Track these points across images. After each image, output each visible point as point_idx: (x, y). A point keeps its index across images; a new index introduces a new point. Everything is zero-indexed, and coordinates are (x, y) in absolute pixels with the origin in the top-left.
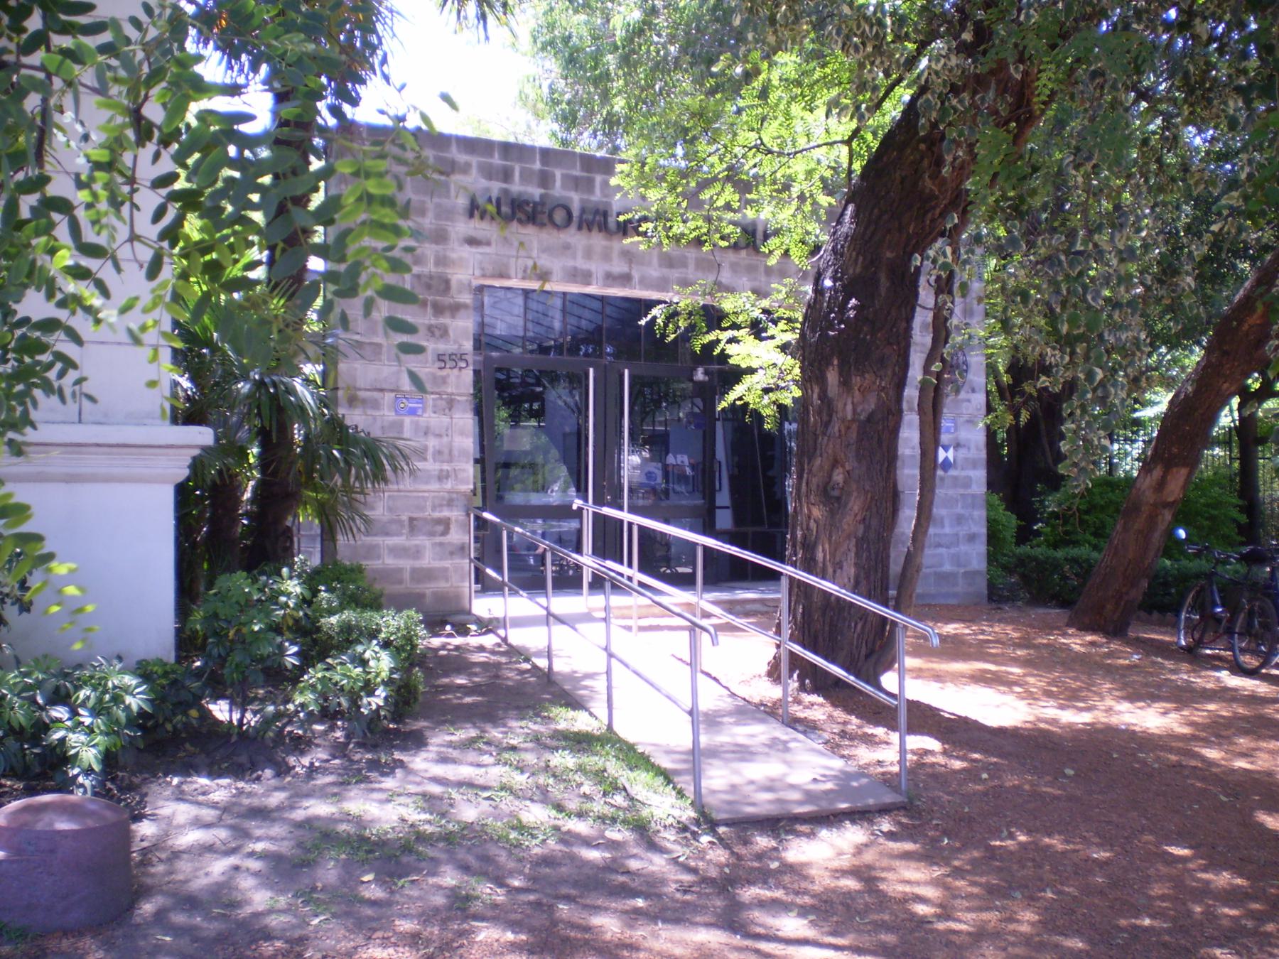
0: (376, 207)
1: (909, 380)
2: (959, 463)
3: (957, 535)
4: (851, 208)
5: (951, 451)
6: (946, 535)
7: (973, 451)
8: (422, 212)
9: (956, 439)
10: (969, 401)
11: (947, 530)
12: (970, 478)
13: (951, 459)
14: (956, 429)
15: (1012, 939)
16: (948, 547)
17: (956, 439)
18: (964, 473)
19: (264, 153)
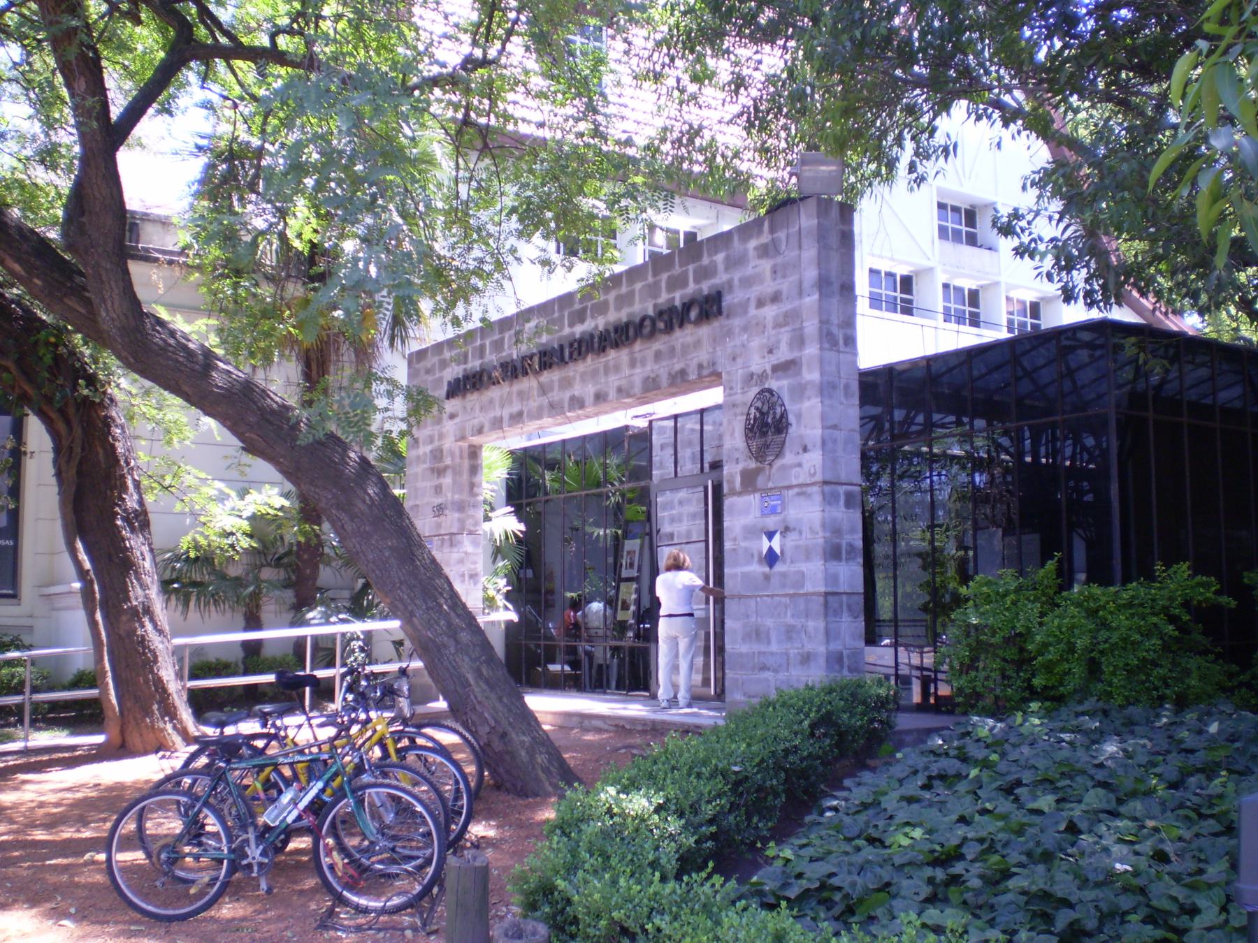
0: (908, 771)
1: (158, 391)
2: (788, 554)
3: (787, 654)
4: (79, 545)
5: (777, 537)
6: (772, 654)
7: (807, 534)
8: (1127, 619)
9: (784, 520)
10: (800, 465)
11: (774, 647)
12: (803, 574)
13: (778, 550)
14: (784, 509)
15: (223, 40)
16: (776, 671)
17: (784, 520)
18: (793, 568)
19: (439, 298)
